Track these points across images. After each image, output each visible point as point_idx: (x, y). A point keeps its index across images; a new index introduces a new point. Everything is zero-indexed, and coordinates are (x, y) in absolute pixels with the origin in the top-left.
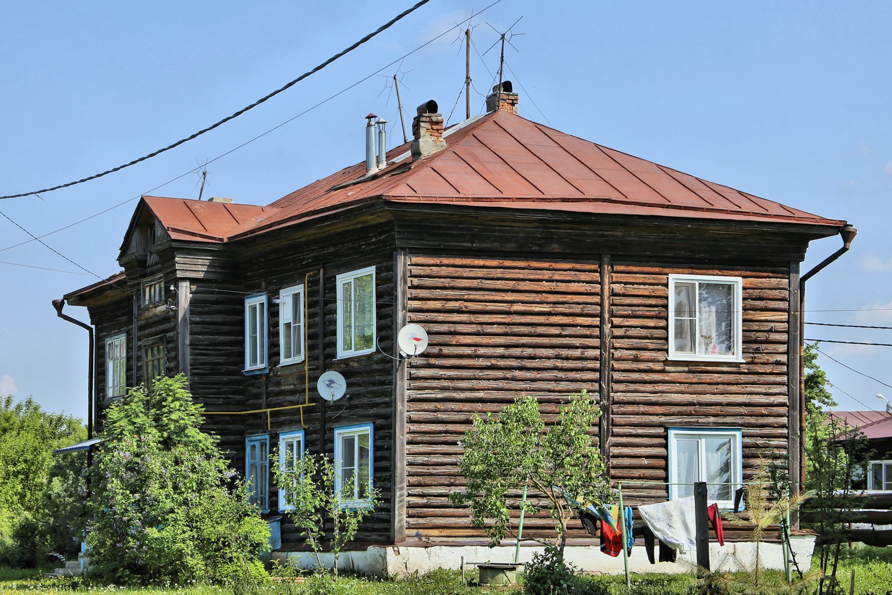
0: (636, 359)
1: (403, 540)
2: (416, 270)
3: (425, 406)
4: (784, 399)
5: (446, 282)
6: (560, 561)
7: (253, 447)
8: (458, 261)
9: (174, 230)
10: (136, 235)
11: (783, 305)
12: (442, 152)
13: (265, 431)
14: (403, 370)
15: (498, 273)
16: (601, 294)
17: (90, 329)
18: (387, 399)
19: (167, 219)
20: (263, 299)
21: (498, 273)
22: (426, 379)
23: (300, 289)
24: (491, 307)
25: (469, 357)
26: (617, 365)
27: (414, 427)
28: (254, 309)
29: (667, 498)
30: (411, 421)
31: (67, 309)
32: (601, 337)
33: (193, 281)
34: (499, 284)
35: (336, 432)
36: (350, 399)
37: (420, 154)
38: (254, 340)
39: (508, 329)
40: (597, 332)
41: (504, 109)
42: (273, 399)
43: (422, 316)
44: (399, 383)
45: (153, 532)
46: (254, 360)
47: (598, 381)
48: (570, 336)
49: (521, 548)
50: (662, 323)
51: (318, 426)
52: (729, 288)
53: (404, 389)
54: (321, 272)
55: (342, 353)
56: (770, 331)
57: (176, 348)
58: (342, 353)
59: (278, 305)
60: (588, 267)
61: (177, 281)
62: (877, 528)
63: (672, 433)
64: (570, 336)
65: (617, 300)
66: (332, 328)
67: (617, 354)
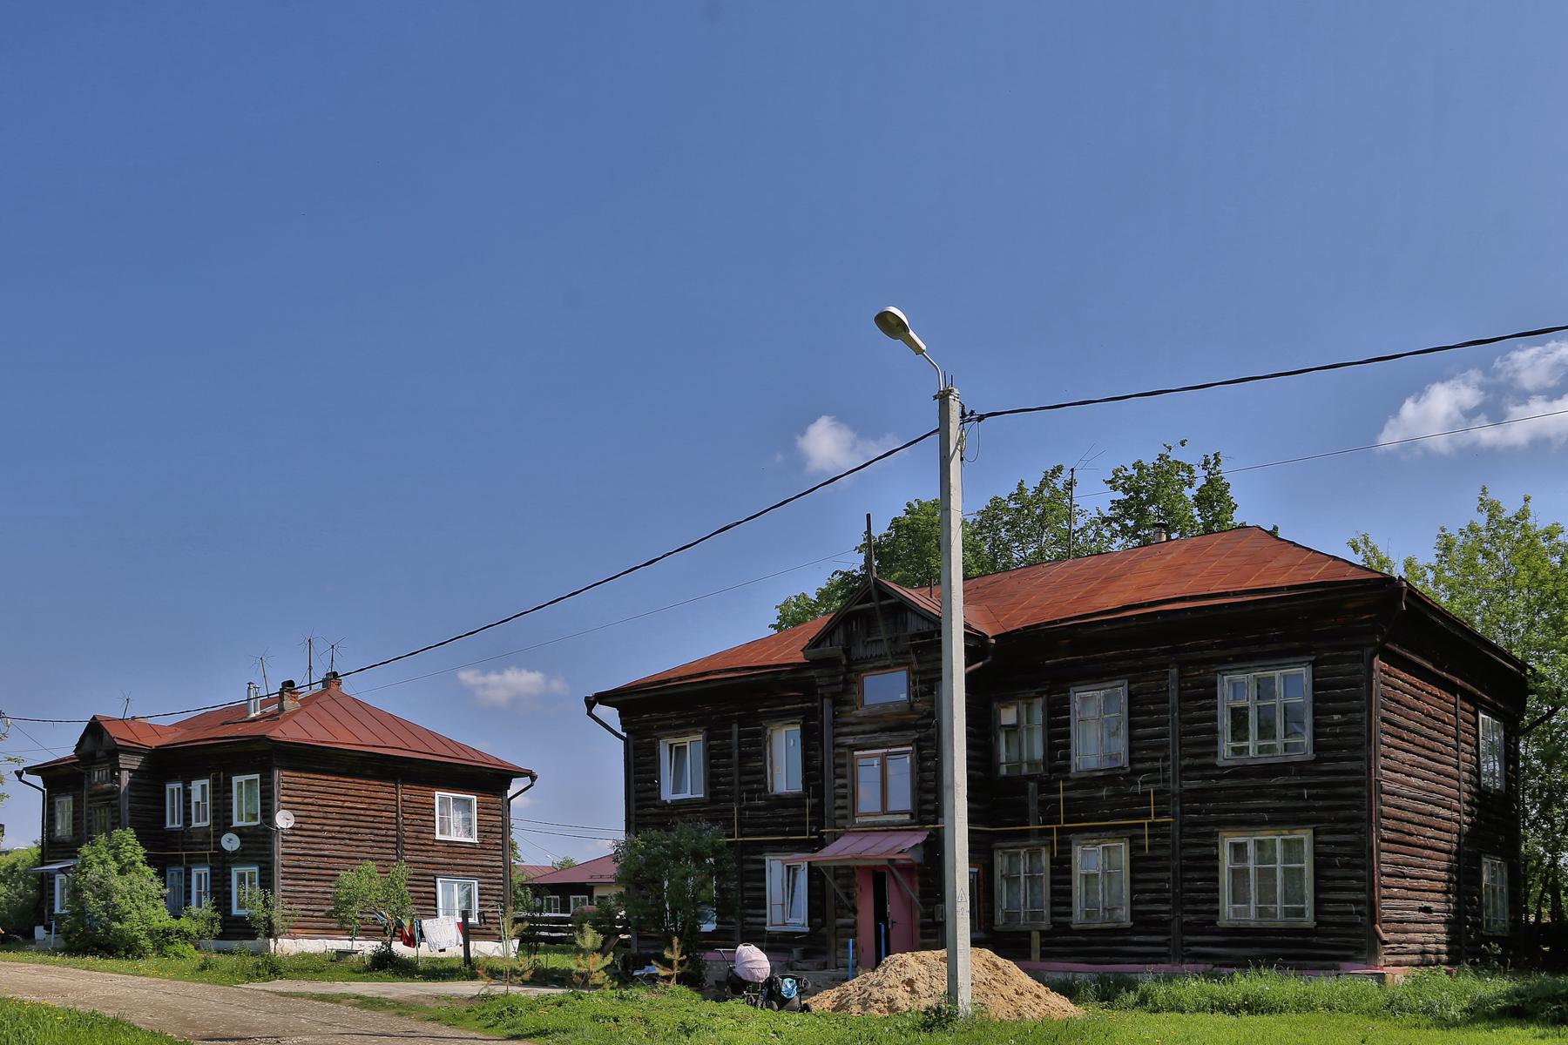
0: (417, 838)
1: (279, 935)
2: (285, 779)
3: (292, 857)
4: (500, 864)
5: (305, 787)
6: (390, 949)
7: (172, 875)
8: (312, 776)
9: (118, 738)
10: (88, 739)
11: (500, 813)
12: (298, 711)
13: (181, 865)
14: (278, 837)
15: (336, 784)
16: (397, 800)
17: (43, 791)
18: (268, 852)
19: (114, 731)
20: (180, 785)
21: (336, 784)
22: (292, 842)
23: (206, 782)
24: (331, 803)
25: (318, 831)
26: (406, 841)
27: (285, 870)
28: (173, 791)
29: (436, 916)
30: (283, 866)
31: (25, 777)
32: (397, 824)
33: (130, 770)
34: (336, 790)
35: (233, 869)
36: (242, 850)
37: (284, 710)
38: (173, 810)
39: (342, 816)
40: (394, 821)
41: (334, 687)
42: (187, 847)
43: (290, 806)
44: (276, 843)
45: (116, 925)
46: (173, 822)
47: (396, 849)
48: (379, 823)
49: (355, 942)
50: (432, 819)
51: (220, 865)
52: (469, 802)
53: (279, 847)
54: (222, 774)
55: (236, 823)
56: (492, 826)
57: (119, 811)
58: (236, 823)
59: (190, 790)
60: (388, 784)
61: (120, 770)
62: (554, 935)
63: (439, 880)
64: (379, 823)
65: (406, 804)
66: (229, 807)
67: (406, 834)
